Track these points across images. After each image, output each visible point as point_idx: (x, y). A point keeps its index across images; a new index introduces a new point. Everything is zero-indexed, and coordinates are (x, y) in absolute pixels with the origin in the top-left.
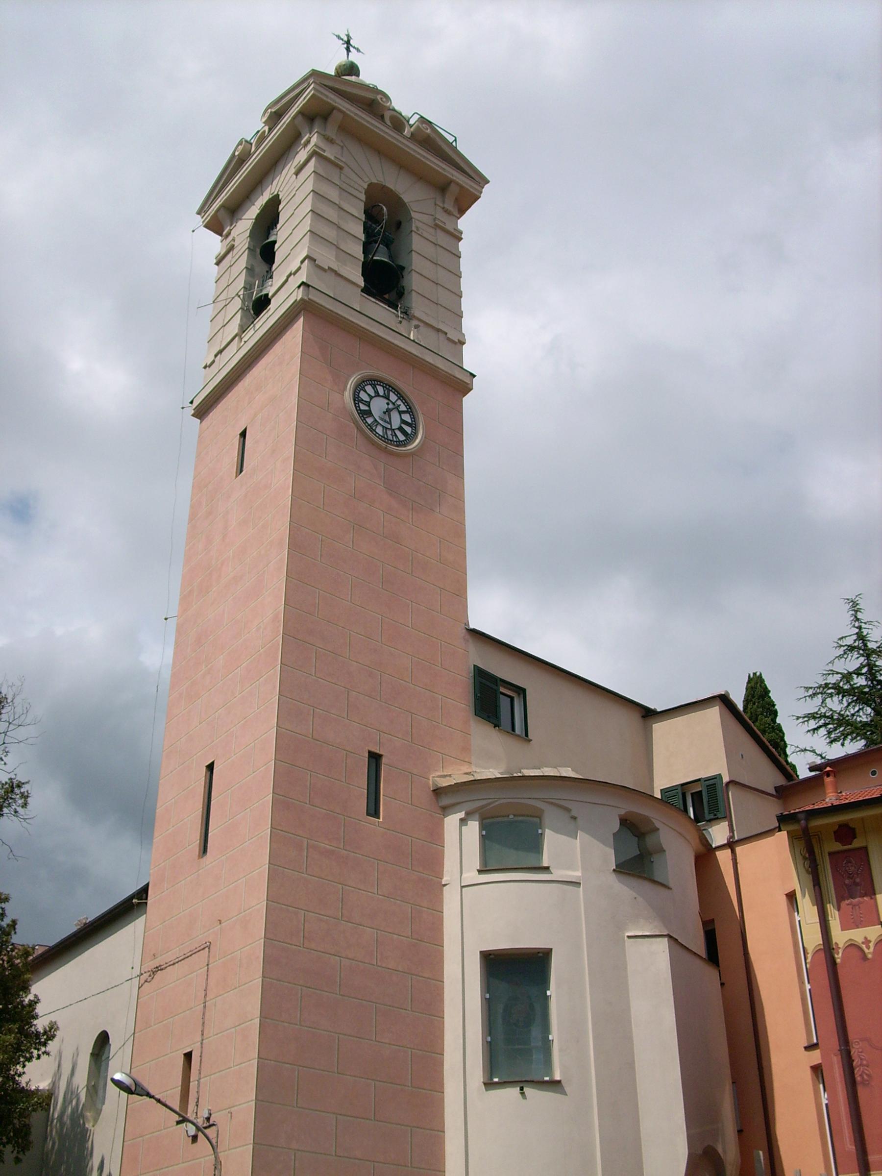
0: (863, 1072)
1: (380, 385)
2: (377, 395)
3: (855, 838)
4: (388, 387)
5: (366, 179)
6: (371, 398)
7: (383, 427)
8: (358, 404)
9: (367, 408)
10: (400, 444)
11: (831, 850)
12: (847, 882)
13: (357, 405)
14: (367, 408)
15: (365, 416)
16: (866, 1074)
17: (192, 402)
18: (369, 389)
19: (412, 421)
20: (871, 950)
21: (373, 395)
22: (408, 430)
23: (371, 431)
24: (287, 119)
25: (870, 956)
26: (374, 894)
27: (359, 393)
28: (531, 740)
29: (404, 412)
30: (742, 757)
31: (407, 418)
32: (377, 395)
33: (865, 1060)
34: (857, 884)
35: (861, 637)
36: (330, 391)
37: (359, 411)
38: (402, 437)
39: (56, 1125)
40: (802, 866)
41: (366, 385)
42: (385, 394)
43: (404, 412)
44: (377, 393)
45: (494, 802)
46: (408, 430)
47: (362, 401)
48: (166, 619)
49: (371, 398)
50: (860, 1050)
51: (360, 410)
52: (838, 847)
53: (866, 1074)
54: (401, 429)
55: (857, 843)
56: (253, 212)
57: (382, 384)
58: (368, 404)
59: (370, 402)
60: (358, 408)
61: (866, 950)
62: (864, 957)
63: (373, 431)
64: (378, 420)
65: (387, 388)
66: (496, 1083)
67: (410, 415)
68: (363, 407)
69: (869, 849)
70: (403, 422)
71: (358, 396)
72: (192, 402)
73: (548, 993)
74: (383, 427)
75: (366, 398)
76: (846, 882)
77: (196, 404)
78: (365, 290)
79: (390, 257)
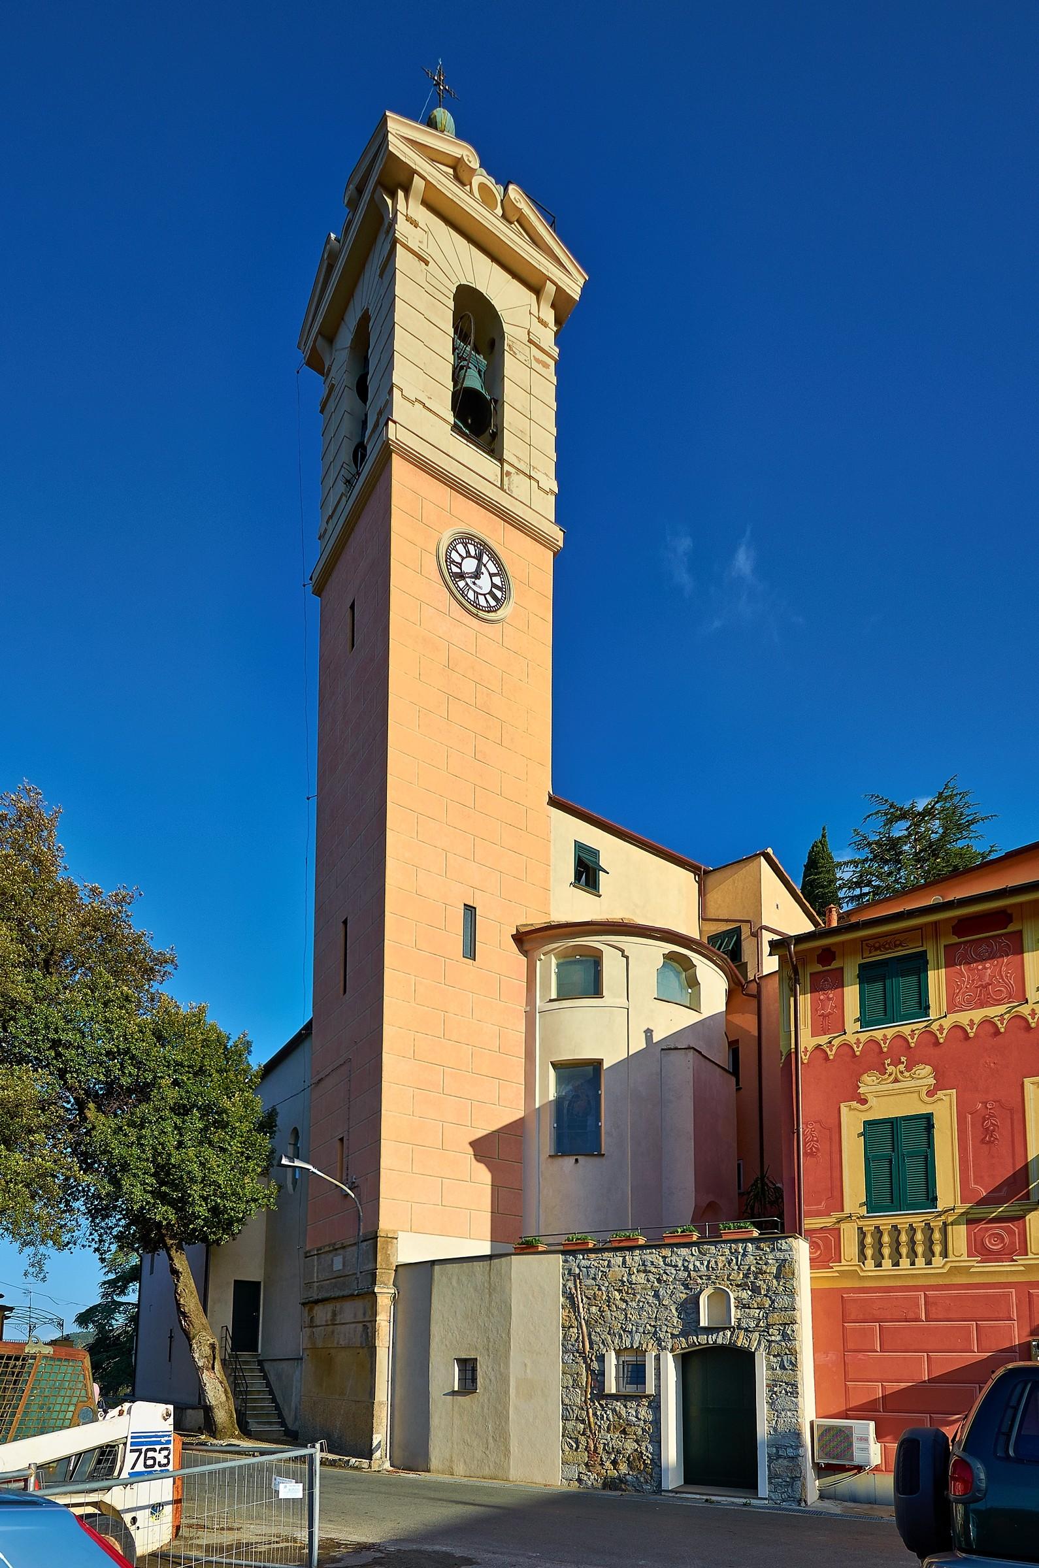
0: (813, 1146)
1: (471, 544)
2: (469, 555)
3: (835, 960)
4: (479, 546)
5: (454, 279)
6: (463, 558)
7: (475, 592)
8: (450, 566)
9: (493, 589)
10: (491, 610)
11: (811, 971)
12: (822, 997)
13: (449, 567)
14: (493, 589)
15: (457, 580)
16: (815, 1147)
17: (311, 579)
18: (460, 548)
19: (502, 585)
20: (833, 1052)
21: (465, 556)
22: (499, 594)
23: (463, 596)
24: (367, 197)
25: (831, 1057)
26: (469, 1018)
27: (450, 554)
28: (601, 896)
29: (495, 575)
30: (778, 908)
31: (497, 580)
32: (469, 555)
33: (816, 1137)
34: (829, 999)
35: (347, 480)
36: (423, 551)
37: (451, 574)
38: (493, 603)
39: (966, 1526)
40: (787, 985)
41: (457, 544)
42: (476, 554)
43: (495, 575)
44: (468, 552)
45: (563, 945)
46: (499, 594)
47: (453, 562)
48: (308, 799)
49: (463, 558)
50: (813, 1130)
51: (452, 572)
52: (820, 968)
53: (815, 1147)
54: (491, 593)
55: (835, 965)
56: (346, 337)
57: (473, 543)
58: (459, 565)
59: (461, 563)
60: (450, 571)
61: (829, 1053)
62: (827, 1058)
63: (464, 596)
64: (470, 584)
65: (478, 548)
66: (560, 1155)
67: (501, 578)
68: (455, 569)
69: (844, 970)
70: (494, 585)
71: (450, 556)
72: (311, 579)
73: (600, 1092)
74: (475, 592)
75: (458, 559)
76: (821, 998)
77: (314, 579)
78: (455, 428)
79: (485, 383)
